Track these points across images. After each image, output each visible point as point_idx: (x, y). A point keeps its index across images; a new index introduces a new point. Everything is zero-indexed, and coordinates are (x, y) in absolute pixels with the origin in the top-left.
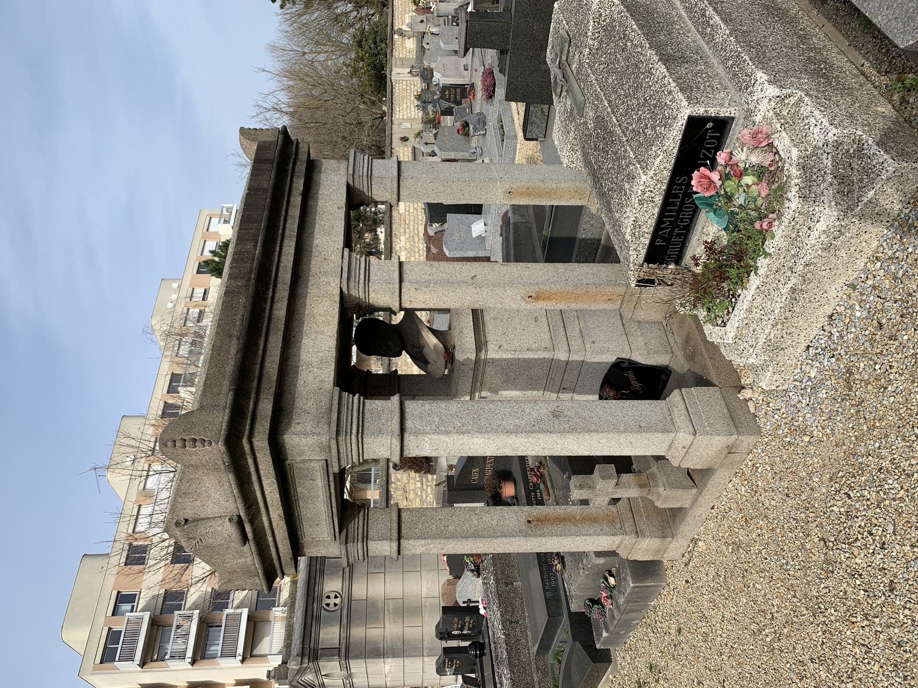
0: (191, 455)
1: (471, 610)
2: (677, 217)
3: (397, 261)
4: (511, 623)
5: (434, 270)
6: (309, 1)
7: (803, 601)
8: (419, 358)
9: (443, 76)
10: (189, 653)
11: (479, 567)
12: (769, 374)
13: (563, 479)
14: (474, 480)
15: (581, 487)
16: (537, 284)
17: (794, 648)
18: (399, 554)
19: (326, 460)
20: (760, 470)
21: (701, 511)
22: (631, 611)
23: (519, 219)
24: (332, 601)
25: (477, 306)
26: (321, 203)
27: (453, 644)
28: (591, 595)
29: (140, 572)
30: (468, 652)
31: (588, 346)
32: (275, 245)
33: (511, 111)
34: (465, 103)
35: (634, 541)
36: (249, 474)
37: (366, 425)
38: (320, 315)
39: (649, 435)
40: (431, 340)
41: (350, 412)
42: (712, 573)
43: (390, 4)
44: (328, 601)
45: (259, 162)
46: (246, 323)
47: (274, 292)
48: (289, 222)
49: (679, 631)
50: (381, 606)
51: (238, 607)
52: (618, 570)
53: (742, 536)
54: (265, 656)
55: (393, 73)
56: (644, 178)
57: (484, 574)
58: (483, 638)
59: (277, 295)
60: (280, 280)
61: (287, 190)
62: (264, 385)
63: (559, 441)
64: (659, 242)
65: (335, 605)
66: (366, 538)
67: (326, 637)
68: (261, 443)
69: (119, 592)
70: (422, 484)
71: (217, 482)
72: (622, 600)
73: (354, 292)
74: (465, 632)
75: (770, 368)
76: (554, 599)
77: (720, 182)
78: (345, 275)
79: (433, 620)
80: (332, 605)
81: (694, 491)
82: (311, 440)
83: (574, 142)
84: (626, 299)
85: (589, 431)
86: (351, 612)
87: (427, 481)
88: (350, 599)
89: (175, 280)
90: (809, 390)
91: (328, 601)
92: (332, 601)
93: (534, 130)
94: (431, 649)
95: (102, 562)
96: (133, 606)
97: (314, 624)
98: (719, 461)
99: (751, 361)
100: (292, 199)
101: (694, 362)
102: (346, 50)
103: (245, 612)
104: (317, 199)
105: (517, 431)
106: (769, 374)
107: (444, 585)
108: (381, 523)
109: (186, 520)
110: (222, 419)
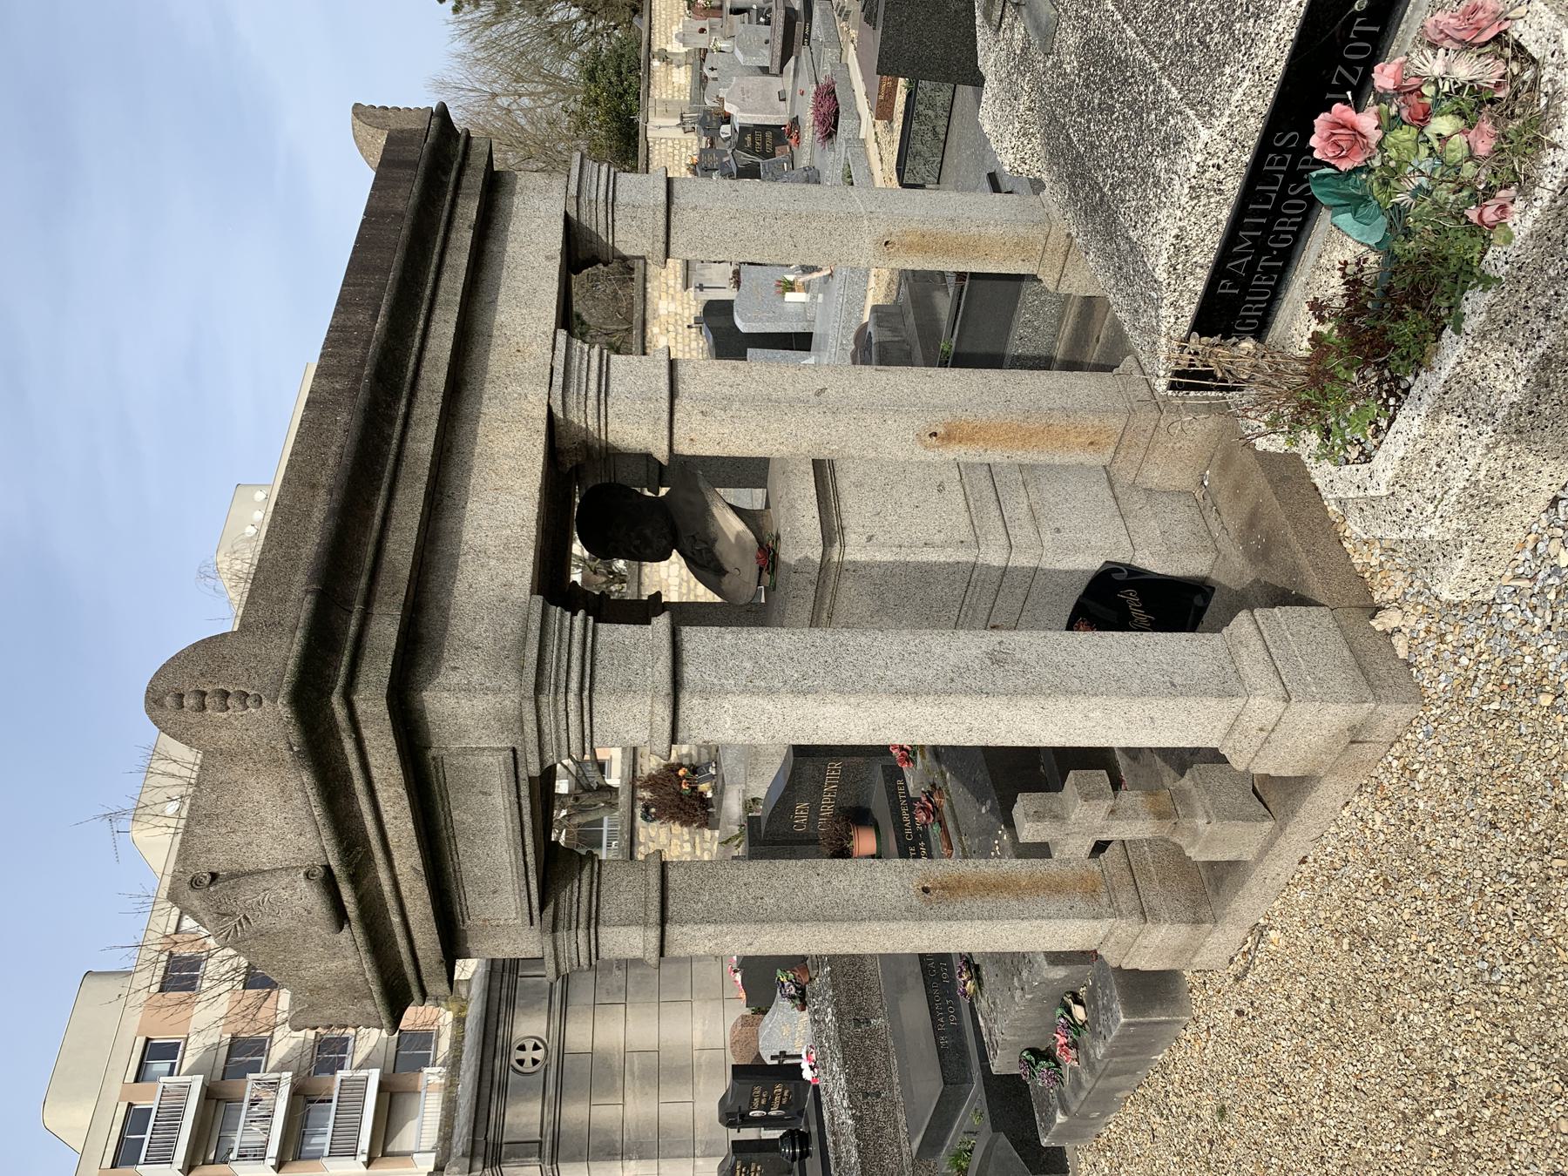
0: (217, 728)
1: (787, 1071)
2: (1266, 229)
3: (665, 357)
4: (866, 1095)
5: (740, 376)
6: (502, 10)
7: (1536, 1049)
8: (706, 565)
9: (742, 111)
10: (273, 1150)
11: (803, 990)
12: (1461, 564)
13: (980, 815)
14: (800, 826)
15: (1038, 816)
16: (949, 407)
17: (1510, 1150)
18: (662, 954)
19: (514, 750)
20: (1421, 776)
21: (1280, 867)
22: (1116, 1073)
23: (888, 336)
24: (528, 1055)
25: (824, 454)
26: (512, 248)
27: (749, 1134)
28: (1033, 1040)
29: (181, 1003)
30: (778, 1150)
31: (1047, 537)
32: (416, 317)
33: (867, 157)
34: (781, 153)
35: (1136, 931)
36: (348, 775)
37: (600, 674)
38: (506, 455)
39: (1191, 702)
40: (732, 525)
41: (565, 646)
42: (1300, 994)
43: (646, 7)
44: (521, 1055)
45: (388, 169)
46: (347, 461)
47: (410, 405)
48: (445, 277)
49: (1222, 1112)
50: (617, 1062)
51: (360, 1067)
52: (1092, 992)
53: (1376, 916)
54: (409, 1154)
55: (649, 126)
56: (1204, 134)
57: (815, 1004)
58: (807, 1123)
59: (417, 412)
60: (423, 383)
61: (444, 218)
62: (383, 587)
63: (1005, 714)
64: (1226, 288)
65: (535, 1062)
66: (594, 920)
67: (517, 1121)
68: (372, 705)
69: (148, 1040)
70: (694, 846)
71: (276, 790)
72: (1100, 1051)
73: (575, 417)
74: (772, 1113)
75: (1466, 551)
76: (956, 1048)
77: (1379, 134)
78: (558, 380)
79: (711, 1092)
80: (528, 1062)
81: (1268, 825)
82: (482, 704)
83: (1029, 116)
84: (1125, 442)
85: (1068, 692)
86: (561, 1074)
87: (703, 840)
88: (561, 1052)
89: (260, 486)
90: (1552, 596)
91: (521, 1055)
92: (528, 1055)
93: (919, 169)
94: (708, 1144)
95: (113, 987)
96: (173, 1065)
97: (495, 1096)
98: (1329, 759)
99: (1428, 531)
100: (453, 236)
101: (1268, 563)
102: (566, 90)
103: (374, 1076)
104: (505, 241)
105: (916, 691)
106: (1461, 564)
107: (735, 1025)
108: (625, 892)
109: (214, 876)
110: (286, 651)
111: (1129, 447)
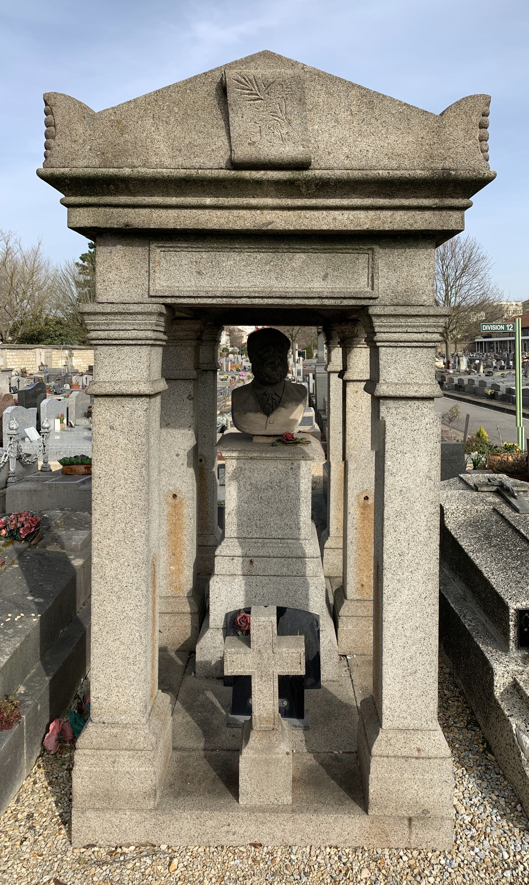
83: (474, 512)
111: (365, 607)
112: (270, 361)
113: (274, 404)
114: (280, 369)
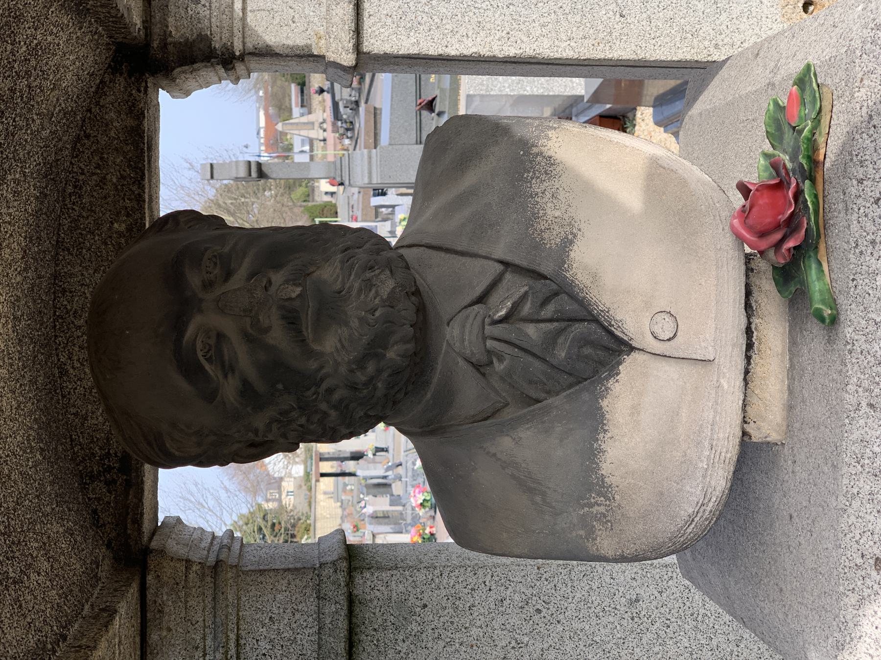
112: (278, 336)
113: (549, 311)
114: (329, 273)
